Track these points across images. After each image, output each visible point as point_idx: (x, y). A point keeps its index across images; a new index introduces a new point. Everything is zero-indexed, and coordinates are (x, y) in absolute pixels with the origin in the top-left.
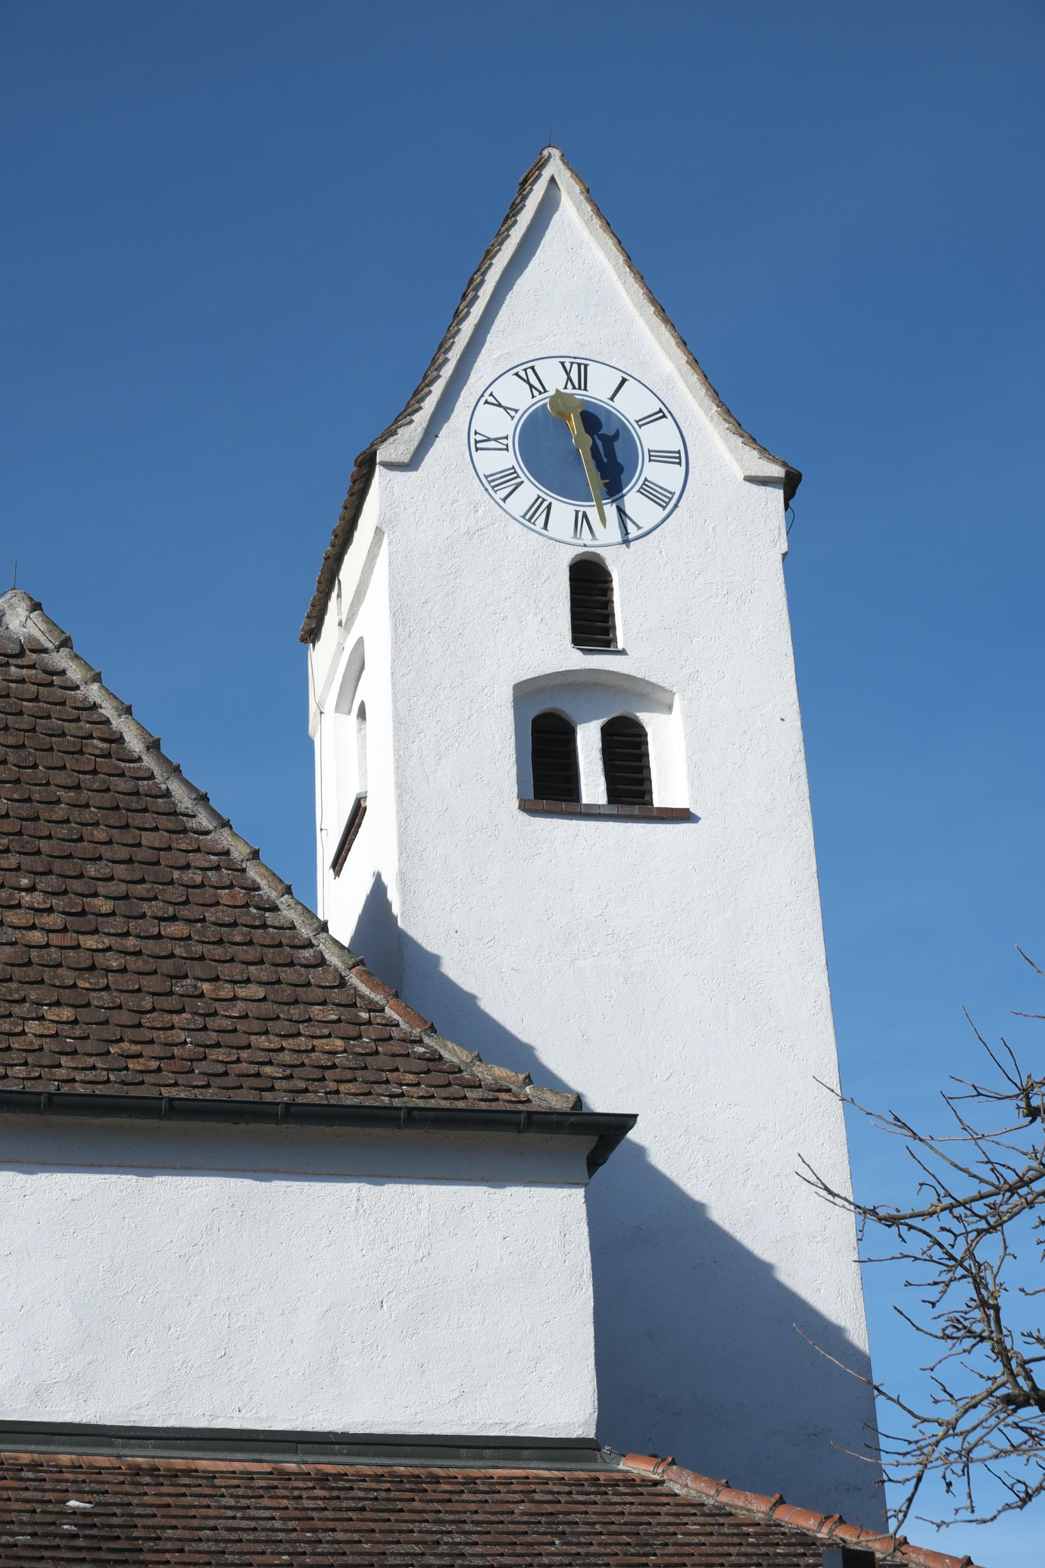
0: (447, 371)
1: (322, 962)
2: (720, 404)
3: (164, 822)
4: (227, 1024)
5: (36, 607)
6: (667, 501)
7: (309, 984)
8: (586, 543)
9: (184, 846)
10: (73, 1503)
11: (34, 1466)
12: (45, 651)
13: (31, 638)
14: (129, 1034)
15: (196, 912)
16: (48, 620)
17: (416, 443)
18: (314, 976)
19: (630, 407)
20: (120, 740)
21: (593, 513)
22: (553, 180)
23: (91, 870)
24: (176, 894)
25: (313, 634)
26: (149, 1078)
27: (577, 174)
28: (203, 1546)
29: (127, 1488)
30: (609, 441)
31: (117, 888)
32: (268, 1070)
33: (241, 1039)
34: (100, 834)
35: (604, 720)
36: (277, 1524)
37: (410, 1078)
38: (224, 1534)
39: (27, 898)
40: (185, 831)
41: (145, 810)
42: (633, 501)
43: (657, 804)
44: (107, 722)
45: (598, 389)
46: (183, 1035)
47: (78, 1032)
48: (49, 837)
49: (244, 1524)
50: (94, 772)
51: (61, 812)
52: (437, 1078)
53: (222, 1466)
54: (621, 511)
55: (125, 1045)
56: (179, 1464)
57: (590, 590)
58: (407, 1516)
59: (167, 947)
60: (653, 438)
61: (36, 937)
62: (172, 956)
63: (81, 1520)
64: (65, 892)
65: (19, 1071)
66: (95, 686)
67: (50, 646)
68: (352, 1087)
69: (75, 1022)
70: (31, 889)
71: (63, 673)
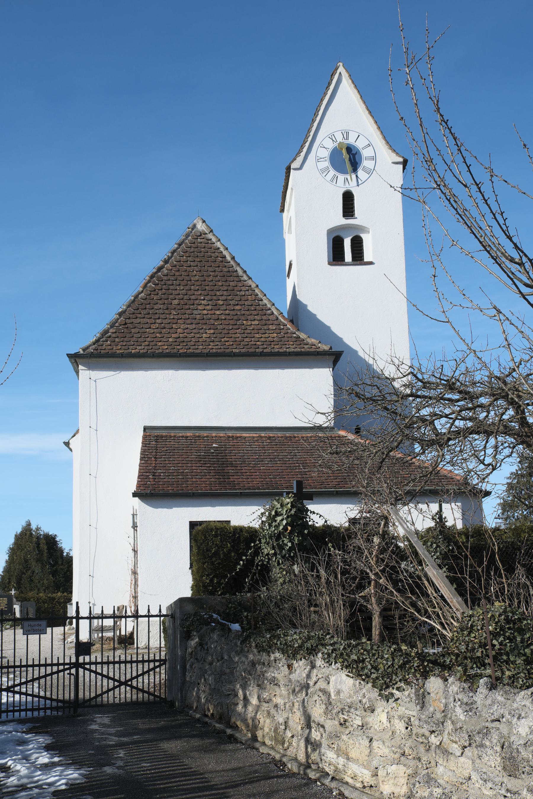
0: (310, 139)
1: (273, 313)
2: (386, 140)
3: (236, 279)
4: (249, 331)
5: (204, 222)
6: (370, 172)
7: (269, 320)
8: (347, 187)
9: (240, 285)
10: (214, 445)
11: (207, 437)
12: (206, 234)
13: (203, 230)
14: (226, 336)
15: (242, 302)
16: (207, 225)
17: (301, 162)
18: (271, 317)
19: (360, 144)
20: (225, 257)
21: (349, 178)
22: (340, 73)
23: (218, 293)
24: (237, 298)
25: (282, 210)
26: (230, 347)
27: (347, 71)
28: (240, 454)
29: (226, 441)
30: (354, 155)
31: (224, 298)
32: (258, 343)
33: (252, 335)
34: (220, 284)
35: (352, 237)
36: (257, 449)
37: (292, 343)
38: (245, 452)
39: (203, 302)
40: (240, 281)
41: (231, 276)
42: (360, 172)
43: (365, 260)
44: (222, 252)
45: (351, 141)
46: (239, 335)
47: (214, 336)
48: (208, 285)
49: (250, 449)
50: (219, 267)
51: (211, 278)
52: (298, 343)
53: (248, 435)
54: (357, 176)
55: (225, 339)
56: (238, 435)
57: (348, 200)
58: (286, 446)
59: (236, 312)
60: (366, 153)
61: (205, 312)
62: (237, 314)
63: (215, 449)
64: (212, 300)
65: (201, 347)
66: (219, 243)
67: (207, 232)
68: (277, 346)
69: (214, 333)
70: (204, 300)
71: (211, 239)
